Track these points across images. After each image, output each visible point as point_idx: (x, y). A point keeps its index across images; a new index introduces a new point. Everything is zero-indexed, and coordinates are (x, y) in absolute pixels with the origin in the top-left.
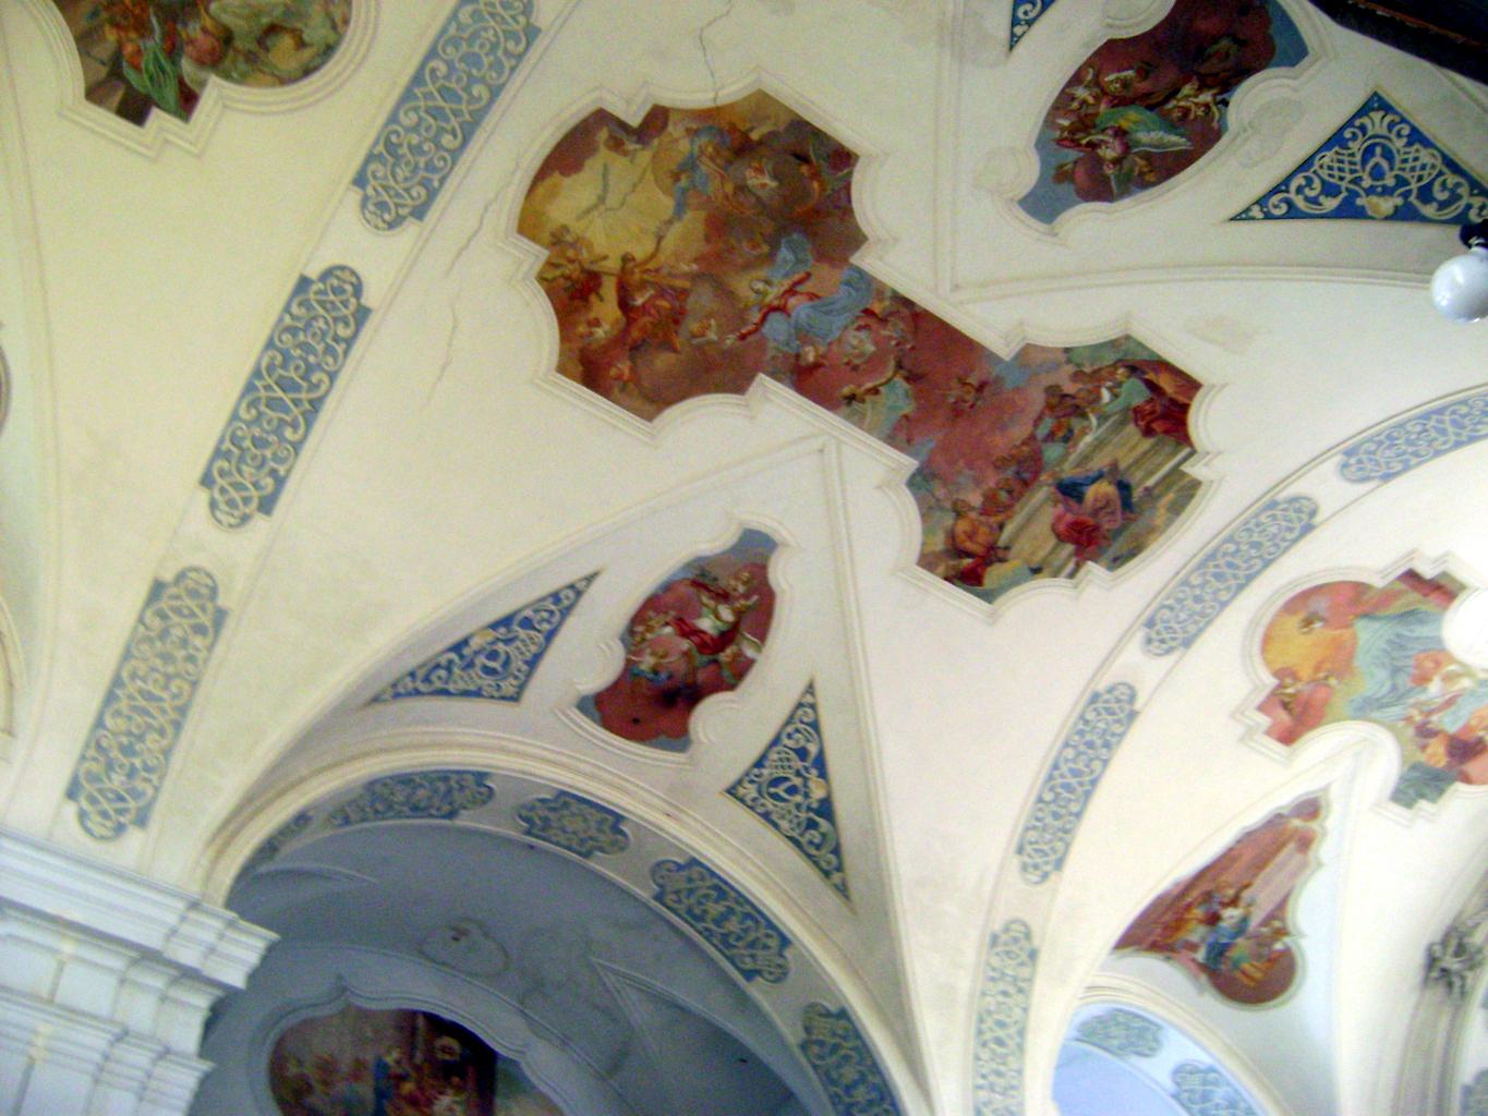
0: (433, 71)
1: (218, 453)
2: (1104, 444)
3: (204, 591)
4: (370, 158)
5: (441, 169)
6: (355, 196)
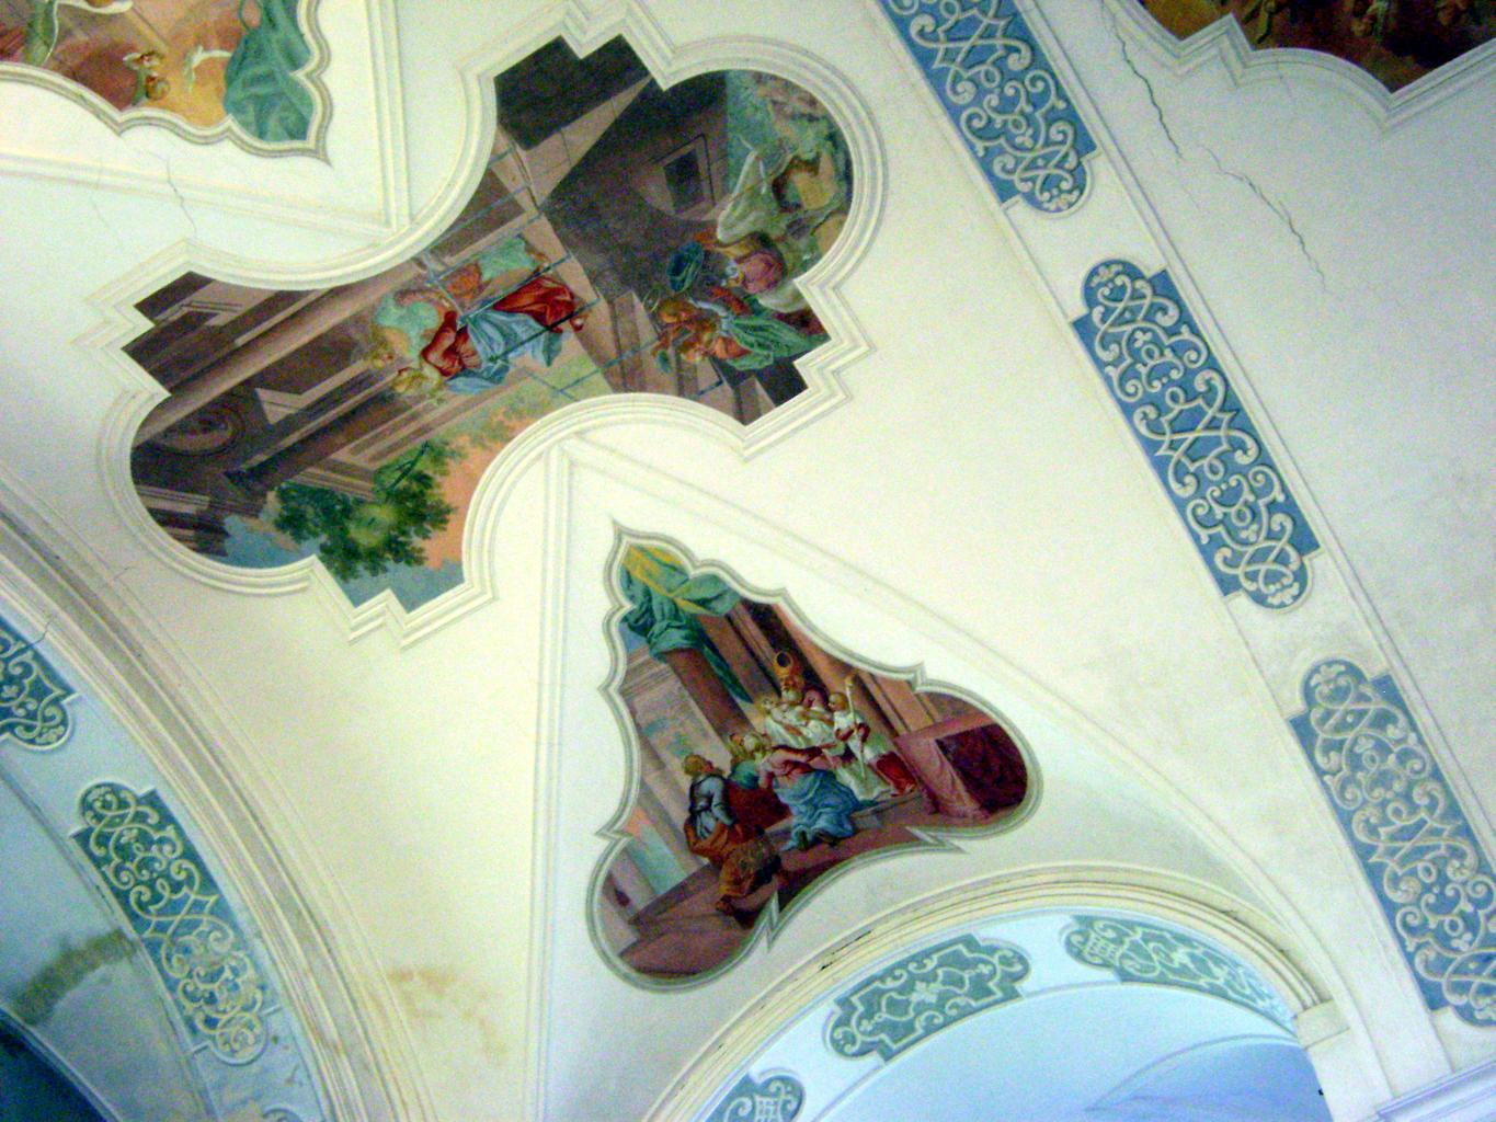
0: (921, 33)
1: (1207, 553)
2: (861, 1030)
3: (1342, 682)
4: (985, 164)
5: (1047, 87)
6: (1020, 209)
